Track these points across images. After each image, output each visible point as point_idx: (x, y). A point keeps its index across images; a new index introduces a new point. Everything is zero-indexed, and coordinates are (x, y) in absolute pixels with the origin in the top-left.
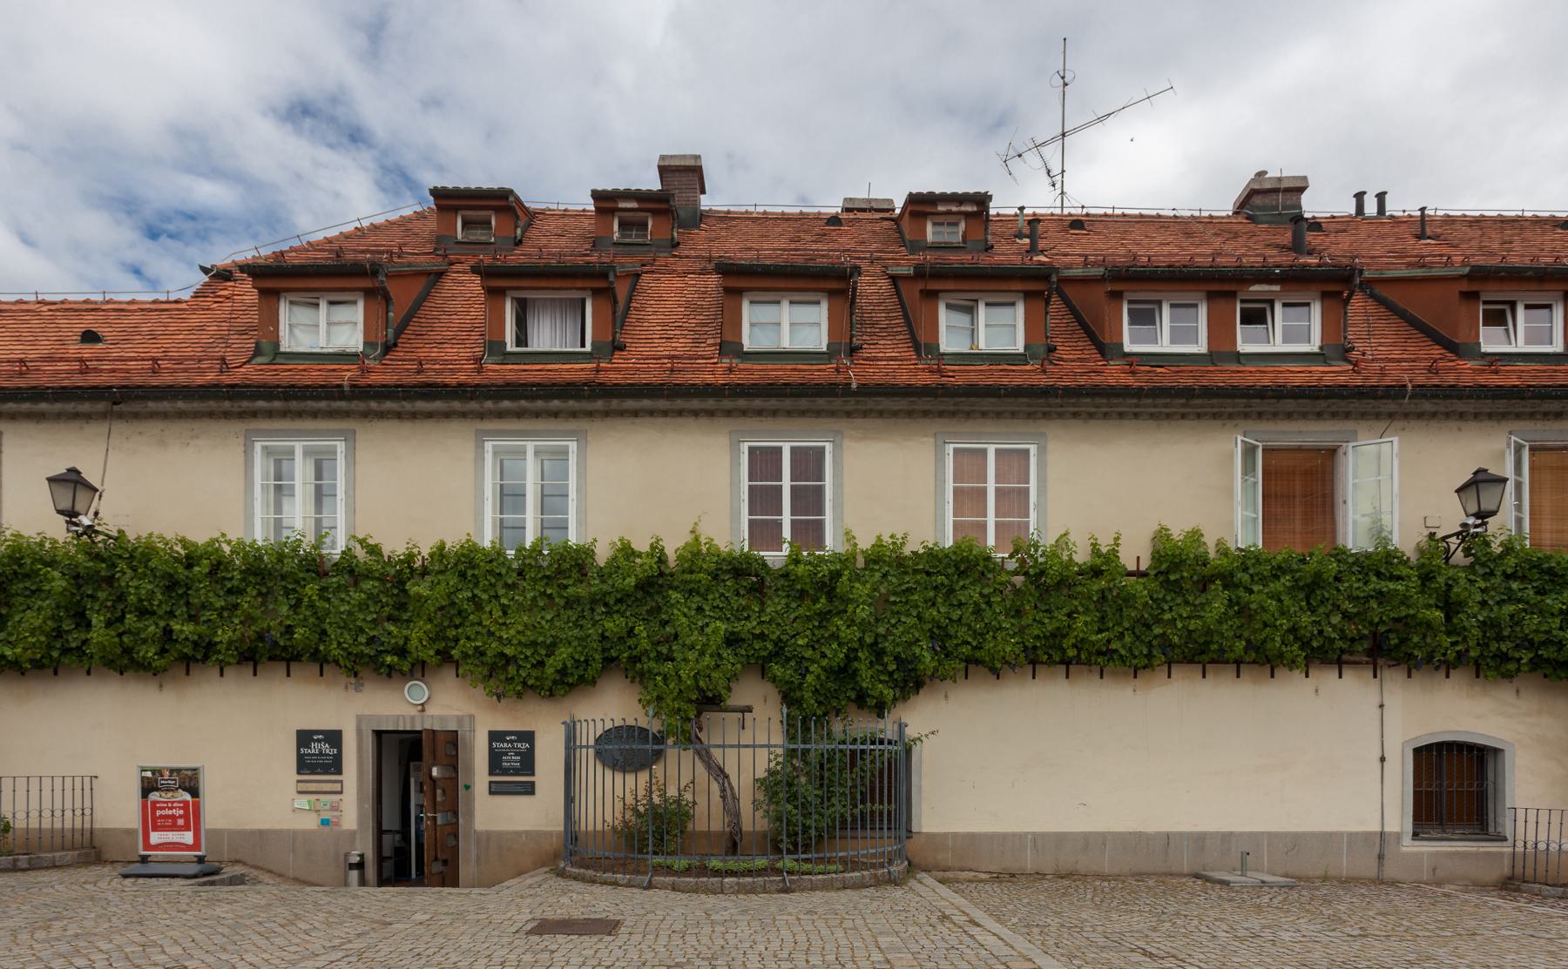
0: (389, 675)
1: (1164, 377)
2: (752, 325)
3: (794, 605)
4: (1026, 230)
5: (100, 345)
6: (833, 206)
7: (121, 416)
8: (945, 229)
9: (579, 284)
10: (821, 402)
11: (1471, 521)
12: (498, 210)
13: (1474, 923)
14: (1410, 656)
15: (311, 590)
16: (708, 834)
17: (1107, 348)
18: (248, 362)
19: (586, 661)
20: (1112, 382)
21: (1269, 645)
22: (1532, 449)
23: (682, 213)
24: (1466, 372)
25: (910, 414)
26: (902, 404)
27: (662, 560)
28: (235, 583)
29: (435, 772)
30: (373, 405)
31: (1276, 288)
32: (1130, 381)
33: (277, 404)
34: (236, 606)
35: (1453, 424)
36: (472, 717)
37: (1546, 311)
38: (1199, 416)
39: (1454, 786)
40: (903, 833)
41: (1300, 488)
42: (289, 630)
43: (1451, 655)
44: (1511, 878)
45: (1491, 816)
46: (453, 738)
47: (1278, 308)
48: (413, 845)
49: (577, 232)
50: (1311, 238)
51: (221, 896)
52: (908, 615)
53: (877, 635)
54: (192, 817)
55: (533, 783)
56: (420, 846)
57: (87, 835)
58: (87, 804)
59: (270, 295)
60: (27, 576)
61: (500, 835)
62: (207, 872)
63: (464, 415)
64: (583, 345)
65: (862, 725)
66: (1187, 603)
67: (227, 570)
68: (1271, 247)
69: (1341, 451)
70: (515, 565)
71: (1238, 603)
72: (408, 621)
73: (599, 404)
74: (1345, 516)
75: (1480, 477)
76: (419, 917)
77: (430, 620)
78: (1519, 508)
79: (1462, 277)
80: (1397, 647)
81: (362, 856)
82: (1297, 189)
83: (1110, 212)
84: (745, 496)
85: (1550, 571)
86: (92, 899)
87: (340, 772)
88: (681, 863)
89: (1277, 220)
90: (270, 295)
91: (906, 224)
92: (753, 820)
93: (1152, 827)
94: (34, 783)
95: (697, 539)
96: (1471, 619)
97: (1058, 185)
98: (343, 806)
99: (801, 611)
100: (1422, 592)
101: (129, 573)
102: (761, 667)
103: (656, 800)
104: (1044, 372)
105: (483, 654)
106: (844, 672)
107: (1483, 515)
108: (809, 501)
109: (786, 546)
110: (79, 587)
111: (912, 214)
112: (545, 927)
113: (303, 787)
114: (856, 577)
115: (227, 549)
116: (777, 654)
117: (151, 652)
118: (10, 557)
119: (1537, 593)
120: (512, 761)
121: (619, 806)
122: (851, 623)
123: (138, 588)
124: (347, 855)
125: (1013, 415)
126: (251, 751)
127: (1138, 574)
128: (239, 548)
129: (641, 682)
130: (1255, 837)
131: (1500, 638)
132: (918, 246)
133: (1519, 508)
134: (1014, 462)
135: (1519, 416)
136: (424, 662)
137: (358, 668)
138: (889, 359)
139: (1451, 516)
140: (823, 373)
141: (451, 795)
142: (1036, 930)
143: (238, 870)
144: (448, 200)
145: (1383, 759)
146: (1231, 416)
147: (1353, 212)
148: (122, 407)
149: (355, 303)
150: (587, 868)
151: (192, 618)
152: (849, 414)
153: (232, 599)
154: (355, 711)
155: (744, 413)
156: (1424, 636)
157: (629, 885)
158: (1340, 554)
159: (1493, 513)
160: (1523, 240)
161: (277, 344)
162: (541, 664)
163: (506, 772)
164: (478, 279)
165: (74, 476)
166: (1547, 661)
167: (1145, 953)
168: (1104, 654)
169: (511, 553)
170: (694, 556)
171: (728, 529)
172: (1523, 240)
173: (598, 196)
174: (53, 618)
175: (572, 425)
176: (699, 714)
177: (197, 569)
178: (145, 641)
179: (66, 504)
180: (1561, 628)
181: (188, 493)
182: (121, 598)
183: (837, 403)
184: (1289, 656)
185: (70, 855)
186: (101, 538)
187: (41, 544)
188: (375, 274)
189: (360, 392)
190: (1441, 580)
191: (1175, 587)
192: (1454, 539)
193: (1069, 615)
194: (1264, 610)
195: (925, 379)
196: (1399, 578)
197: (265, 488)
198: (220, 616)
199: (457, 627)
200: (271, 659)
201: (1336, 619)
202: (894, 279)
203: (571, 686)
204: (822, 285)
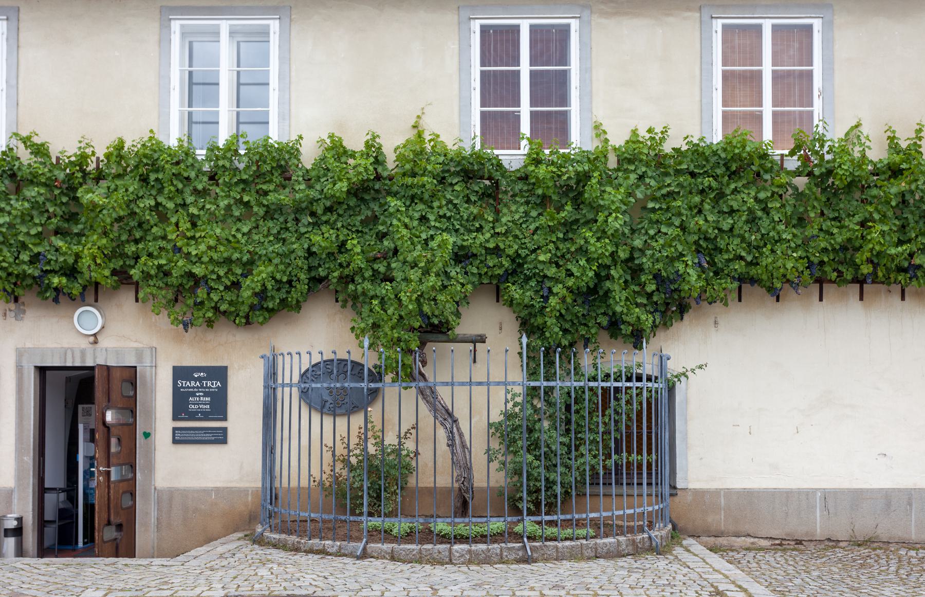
0: (56, 300)
3: (534, 213)
16: (432, 491)
19: (290, 282)
27: (378, 161)
36: (154, 350)
46: (130, 375)
52: (670, 225)
53: (633, 248)
55: (224, 430)
61: (185, 493)
65: (616, 358)
70: (206, 168)
72: (80, 235)
77: (105, 234)
84: (476, 84)
88: (400, 525)
92: (488, 475)
95: (420, 135)
103: (372, 450)
105: (167, 274)
106: (593, 294)
108: (552, 88)
109: (524, 143)
114: (608, 179)
116: (514, 272)
120: (200, 402)
121: (328, 456)
122: (602, 234)
129: (354, 306)
136: (97, 284)
137: (19, 291)
141: (126, 444)
157: (340, 554)
162: (236, 285)
163: (192, 416)
170: (416, 155)
171: (458, 127)
176: (423, 344)
193: (862, 224)
199: (137, 242)
203: (271, 311)
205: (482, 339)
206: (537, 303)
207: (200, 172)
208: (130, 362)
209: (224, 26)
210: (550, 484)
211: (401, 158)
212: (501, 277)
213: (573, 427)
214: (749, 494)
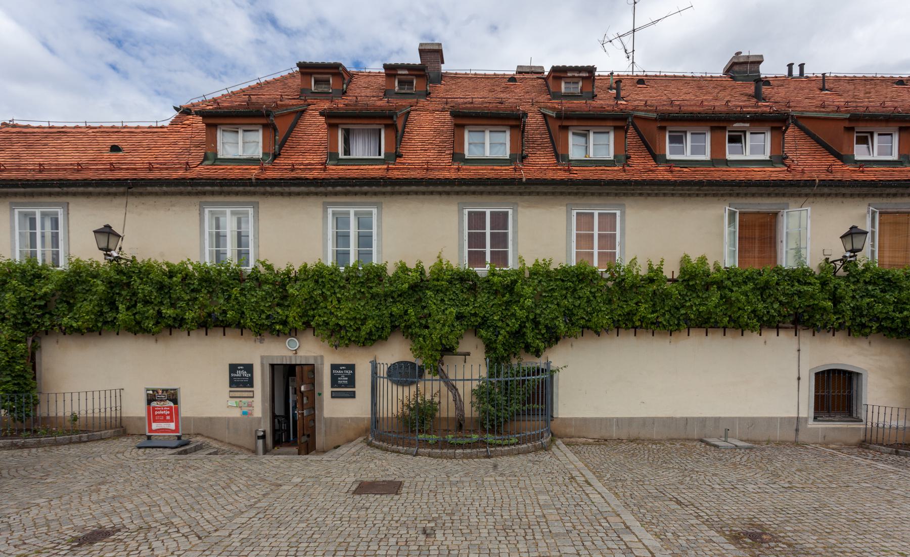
0: (278, 335)
1: (687, 174)
2: (470, 144)
3: (492, 298)
4: (614, 85)
5: (121, 154)
6: (511, 70)
7: (132, 194)
8: (572, 86)
9: (378, 122)
10: (506, 188)
11: (848, 254)
12: (333, 74)
13: (847, 477)
14: (814, 325)
15: (235, 291)
16: (447, 419)
17: (659, 158)
18: (201, 164)
19: (382, 328)
20: (660, 177)
21: (741, 320)
22: (880, 213)
23: (432, 75)
24: (844, 172)
25: (553, 194)
26: (550, 189)
27: (422, 273)
28: (195, 286)
29: (303, 388)
30: (268, 189)
31: (748, 125)
32: (668, 176)
33: (217, 188)
34: (196, 299)
35: (840, 200)
36: (322, 357)
37: (889, 137)
38: (706, 195)
39: (836, 392)
40: (549, 419)
41: (759, 233)
42: (225, 312)
43: (836, 325)
44: (864, 441)
45: (854, 408)
46: (312, 368)
47: (748, 135)
48: (291, 427)
49: (376, 86)
50: (765, 90)
51: (192, 463)
52: (552, 303)
53: (536, 314)
54: (174, 414)
55: (354, 392)
56: (295, 422)
57: (118, 420)
58: (118, 404)
59: (212, 127)
60: (84, 282)
61: (338, 419)
62: (183, 445)
63: (316, 194)
64: (380, 155)
65: (530, 361)
66: (698, 296)
67: (190, 279)
68: (745, 100)
69: (780, 214)
70: (344, 275)
71: (725, 297)
72: (288, 306)
73: (389, 189)
74: (782, 249)
75: (853, 231)
76: (297, 480)
77: (299, 306)
78: (873, 246)
79: (846, 119)
80: (808, 320)
81: (264, 432)
82: (758, 61)
83: (658, 74)
84: (466, 238)
85: (889, 280)
86: (122, 466)
87: (252, 386)
88: (433, 438)
89: (746, 79)
90: (212, 127)
91: (550, 81)
92: (470, 411)
93: (679, 415)
94: (90, 395)
95: (441, 261)
96: (847, 306)
97: (631, 58)
98: (254, 404)
99: (496, 301)
100: (822, 291)
101: (138, 281)
102: (475, 330)
103: (419, 401)
104: (625, 171)
105: (327, 324)
106: (518, 334)
107: (854, 251)
108: (500, 240)
109: (488, 266)
110: (112, 288)
111: (554, 77)
112: (364, 488)
113: (233, 394)
114: (525, 282)
115: (190, 267)
116: (483, 324)
117: (150, 324)
118: (74, 272)
119: (881, 292)
120: (343, 380)
121: (400, 404)
122: (522, 308)
123: (143, 289)
124: (256, 431)
125: (608, 194)
126: (203, 376)
127: (673, 281)
128: (198, 268)
129: (411, 338)
130: (732, 420)
131: (861, 316)
132: (557, 95)
133: (873, 246)
134: (608, 221)
135: (874, 195)
136: (296, 329)
137: (261, 332)
138: (541, 164)
139: (838, 251)
140: (506, 172)
141: (311, 400)
142: (620, 484)
143: (200, 439)
144: (306, 69)
145: (799, 379)
146: (722, 195)
147: (786, 73)
148: (134, 190)
149: (257, 131)
150: (384, 442)
151: (173, 305)
152: (521, 194)
153: (194, 295)
154: (260, 353)
155: (465, 193)
156: (822, 315)
157: (406, 453)
158: (778, 270)
159: (860, 250)
160: (877, 92)
161: (216, 154)
162: (359, 329)
163: (340, 386)
164: (323, 119)
165: (108, 230)
166: (886, 328)
167: (679, 503)
168: (654, 324)
169: (342, 269)
170: (439, 271)
171: (457, 258)
172: (877, 92)
173: (387, 67)
174: (98, 305)
175: (375, 199)
176: (442, 356)
177: (175, 279)
178: (147, 318)
179: (104, 245)
180: (894, 311)
181: (170, 237)
182: (134, 294)
183: (515, 188)
184: (751, 325)
185: (110, 432)
186: (123, 261)
187: (91, 265)
188: (268, 116)
189: (261, 182)
190: (832, 285)
191: (692, 289)
192: (838, 263)
193: (637, 304)
194: (739, 301)
195: (561, 175)
196: (810, 284)
197: (210, 234)
198: (188, 304)
199: (314, 310)
200: (215, 326)
201: (776, 306)
202: (545, 116)
203: (374, 341)
204: (506, 123)
205: (468, 354)
206: (493, 338)
207: (342, 278)
208: (311, 362)
209: (352, 211)
210: (498, 417)
211: (432, 272)
212: (478, 326)
213: (509, 392)
214: (585, 420)
